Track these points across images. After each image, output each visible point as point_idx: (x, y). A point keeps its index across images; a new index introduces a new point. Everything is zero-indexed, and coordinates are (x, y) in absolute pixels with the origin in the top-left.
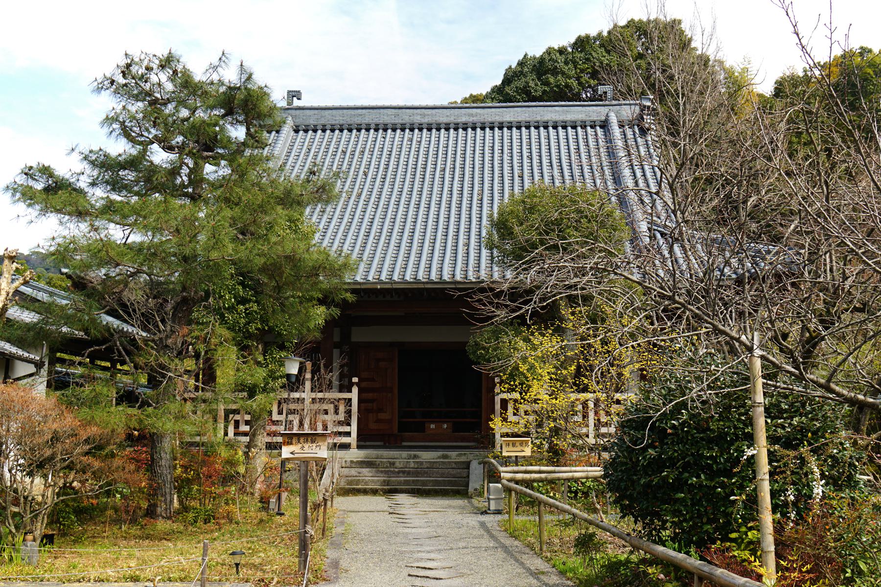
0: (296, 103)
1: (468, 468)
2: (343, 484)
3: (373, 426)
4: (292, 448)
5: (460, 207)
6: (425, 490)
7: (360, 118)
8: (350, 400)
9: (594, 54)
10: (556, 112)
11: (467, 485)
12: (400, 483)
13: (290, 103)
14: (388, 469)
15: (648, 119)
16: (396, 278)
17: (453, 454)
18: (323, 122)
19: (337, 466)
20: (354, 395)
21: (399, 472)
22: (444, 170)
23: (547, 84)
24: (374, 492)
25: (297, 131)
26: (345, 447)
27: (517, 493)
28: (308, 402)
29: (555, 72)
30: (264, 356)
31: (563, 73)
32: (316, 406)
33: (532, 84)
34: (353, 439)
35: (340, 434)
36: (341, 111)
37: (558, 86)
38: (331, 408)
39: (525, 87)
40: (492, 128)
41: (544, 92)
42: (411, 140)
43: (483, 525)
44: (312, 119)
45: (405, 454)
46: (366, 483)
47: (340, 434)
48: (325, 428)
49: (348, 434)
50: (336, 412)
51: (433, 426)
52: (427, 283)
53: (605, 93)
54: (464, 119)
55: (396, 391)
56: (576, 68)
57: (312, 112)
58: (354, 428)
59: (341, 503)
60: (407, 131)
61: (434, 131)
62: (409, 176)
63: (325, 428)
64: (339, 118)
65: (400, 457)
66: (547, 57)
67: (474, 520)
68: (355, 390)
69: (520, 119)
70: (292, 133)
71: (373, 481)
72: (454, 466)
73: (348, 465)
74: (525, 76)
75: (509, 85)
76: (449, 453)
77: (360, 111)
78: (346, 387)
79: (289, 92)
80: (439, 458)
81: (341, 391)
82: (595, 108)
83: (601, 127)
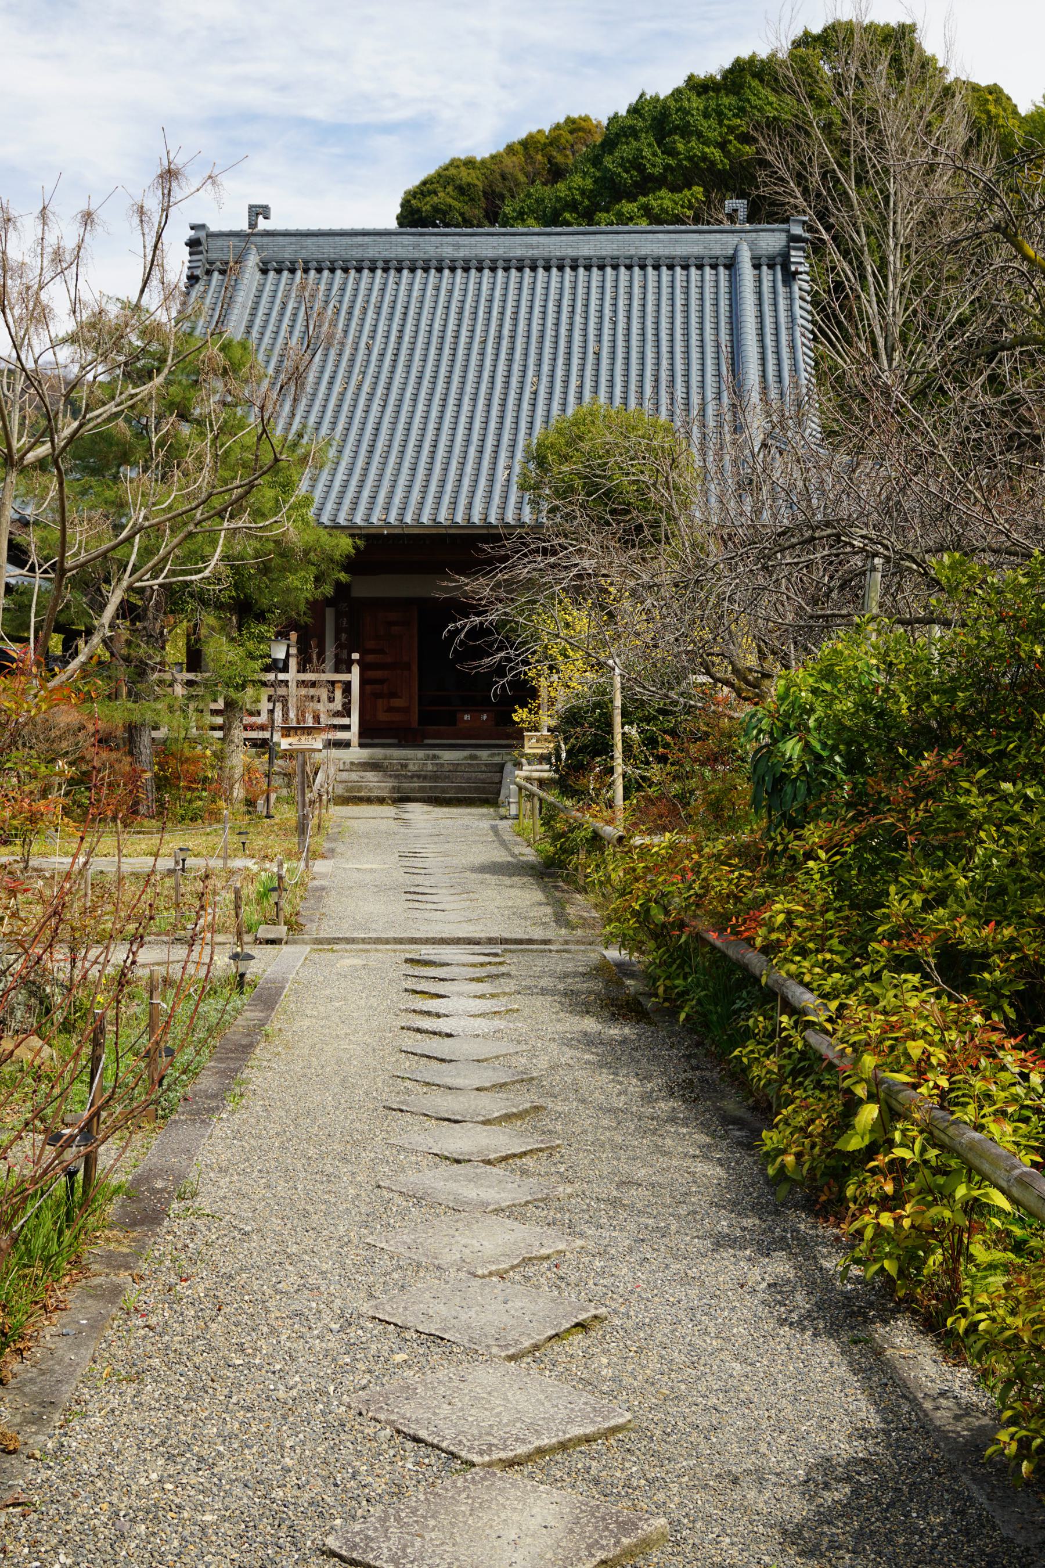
0: (263, 224)
1: (501, 771)
2: (340, 790)
3: (383, 717)
4: (290, 740)
5: (503, 405)
6: (444, 799)
7: (360, 250)
8: (350, 682)
9: (752, 98)
10: (659, 241)
11: (498, 793)
12: (413, 790)
13: (253, 225)
14: (398, 773)
15: (796, 256)
16: (408, 519)
17: (484, 754)
18: (304, 254)
19: (332, 770)
20: (354, 676)
21: (412, 777)
22: (484, 342)
23: (672, 152)
24: (381, 801)
25: (264, 272)
26: (347, 744)
27: (540, 800)
28: (293, 685)
29: (686, 131)
30: (240, 630)
31: (700, 135)
32: (304, 691)
33: (647, 153)
34: (353, 735)
35: (335, 727)
36: (330, 239)
37: (690, 159)
38: (324, 693)
39: (635, 158)
40: (561, 268)
41: (668, 168)
42: (437, 289)
43: (494, 828)
44: (287, 251)
45: (421, 753)
46: (370, 790)
47: (335, 727)
48: (317, 718)
49: (347, 728)
50: (331, 700)
51: (467, 717)
52: (450, 527)
53: (735, 211)
54: (519, 253)
55: (415, 668)
56: (721, 123)
57: (288, 239)
58: (354, 720)
59: (338, 811)
60: (433, 271)
61: (473, 271)
62: (433, 351)
63: (317, 718)
64: (328, 250)
65: (415, 758)
66: (672, 104)
67: (486, 824)
68: (356, 669)
69: (604, 253)
70: (258, 275)
71: (379, 788)
72: (484, 768)
73: (347, 767)
74: (637, 138)
75: (611, 153)
76: (479, 753)
77: (360, 239)
78: (343, 665)
79: (251, 207)
80: (465, 758)
81: (337, 671)
82: (718, 236)
83: (727, 267)
